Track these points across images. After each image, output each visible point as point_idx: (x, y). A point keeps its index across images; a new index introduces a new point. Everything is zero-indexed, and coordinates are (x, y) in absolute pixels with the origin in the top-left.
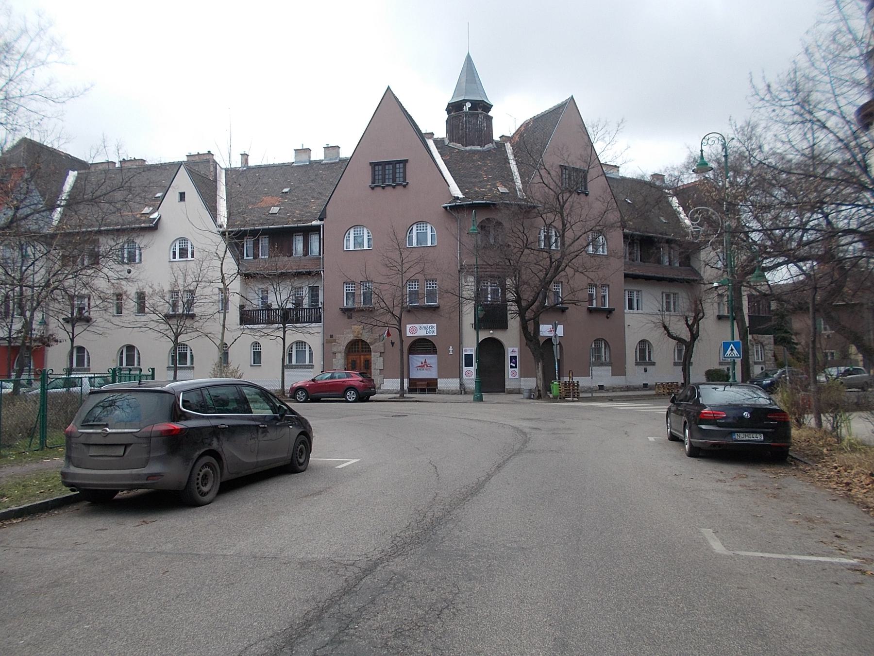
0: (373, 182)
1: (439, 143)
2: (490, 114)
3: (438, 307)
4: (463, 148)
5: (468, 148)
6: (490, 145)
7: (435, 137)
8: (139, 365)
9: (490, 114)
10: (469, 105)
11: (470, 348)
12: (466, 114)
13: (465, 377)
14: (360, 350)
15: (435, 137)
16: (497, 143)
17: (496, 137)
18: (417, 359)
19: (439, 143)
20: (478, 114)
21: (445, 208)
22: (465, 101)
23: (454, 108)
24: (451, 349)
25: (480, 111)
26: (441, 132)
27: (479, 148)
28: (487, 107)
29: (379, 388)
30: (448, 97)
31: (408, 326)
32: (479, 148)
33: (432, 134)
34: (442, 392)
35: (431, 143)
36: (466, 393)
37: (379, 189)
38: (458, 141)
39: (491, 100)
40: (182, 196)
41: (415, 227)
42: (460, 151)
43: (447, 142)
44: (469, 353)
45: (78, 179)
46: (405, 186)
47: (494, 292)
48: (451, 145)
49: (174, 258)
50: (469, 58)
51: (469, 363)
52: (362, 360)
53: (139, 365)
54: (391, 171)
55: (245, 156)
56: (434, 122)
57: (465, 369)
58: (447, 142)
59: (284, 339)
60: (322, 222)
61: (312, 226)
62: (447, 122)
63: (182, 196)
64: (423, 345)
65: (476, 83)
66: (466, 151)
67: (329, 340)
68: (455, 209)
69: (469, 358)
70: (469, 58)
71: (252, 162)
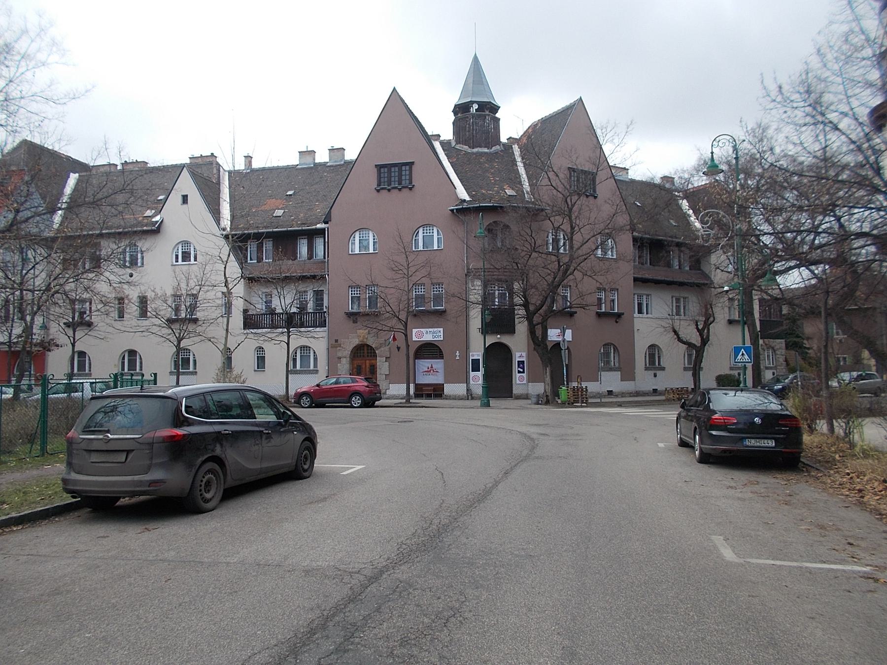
0: (379, 185)
1: (445, 145)
2: (497, 115)
3: (444, 312)
4: (470, 150)
5: (475, 150)
6: (498, 147)
7: (441, 139)
8: (141, 370)
9: (497, 115)
10: (475, 106)
11: (477, 353)
12: (473, 115)
13: (471, 382)
14: (366, 354)
15: (441, 139)
16: (504, 145)
17: (503, 139)
18: (424, 364)
19: (445, 145)
20: (485, 116)
21: (452, 211)
22: (472, 102)
23: (461, 110)
24: (458, 354)
25: (487, 112)
26: (447, 134)
27: (486, 150)
28: (495, 109)
29: (385, 393)
30: (454, 98)
31: (414, 331)
32: (486, 150)
33: (439, 136)
34: (448, 398)
35: (437, 145)
36: (472, 398)
37: (384, 192)
38: (465, 143)
39: (498, 101)
40: (185, 199)
41: (421, 230)
42: (466, 153)
43: (453, 144)
44: (476, 357)
45: (79, 182)
46: (411, 189)
47: (502, 296)
48: (458, 147)
49: (177, 261)
50: (476, 59)
51: (476, 368)
52: (368, 365)
53: (141, 370)
54: (397, 174)
55: (248, 158)
56: (440, 124)
57: (472, 374)
58: (453, 144)
59: (288, 344)
60: (327, 225)
61: (316, 229)
62: (453, 123)
63: (185, 199)
64: (429, 350)
65: (483, 84)
66: (473, 153)
67: (334, 345)
68: (462, 212)
69: (476, 363)
70: (476, 59)
71: (256, 165)
